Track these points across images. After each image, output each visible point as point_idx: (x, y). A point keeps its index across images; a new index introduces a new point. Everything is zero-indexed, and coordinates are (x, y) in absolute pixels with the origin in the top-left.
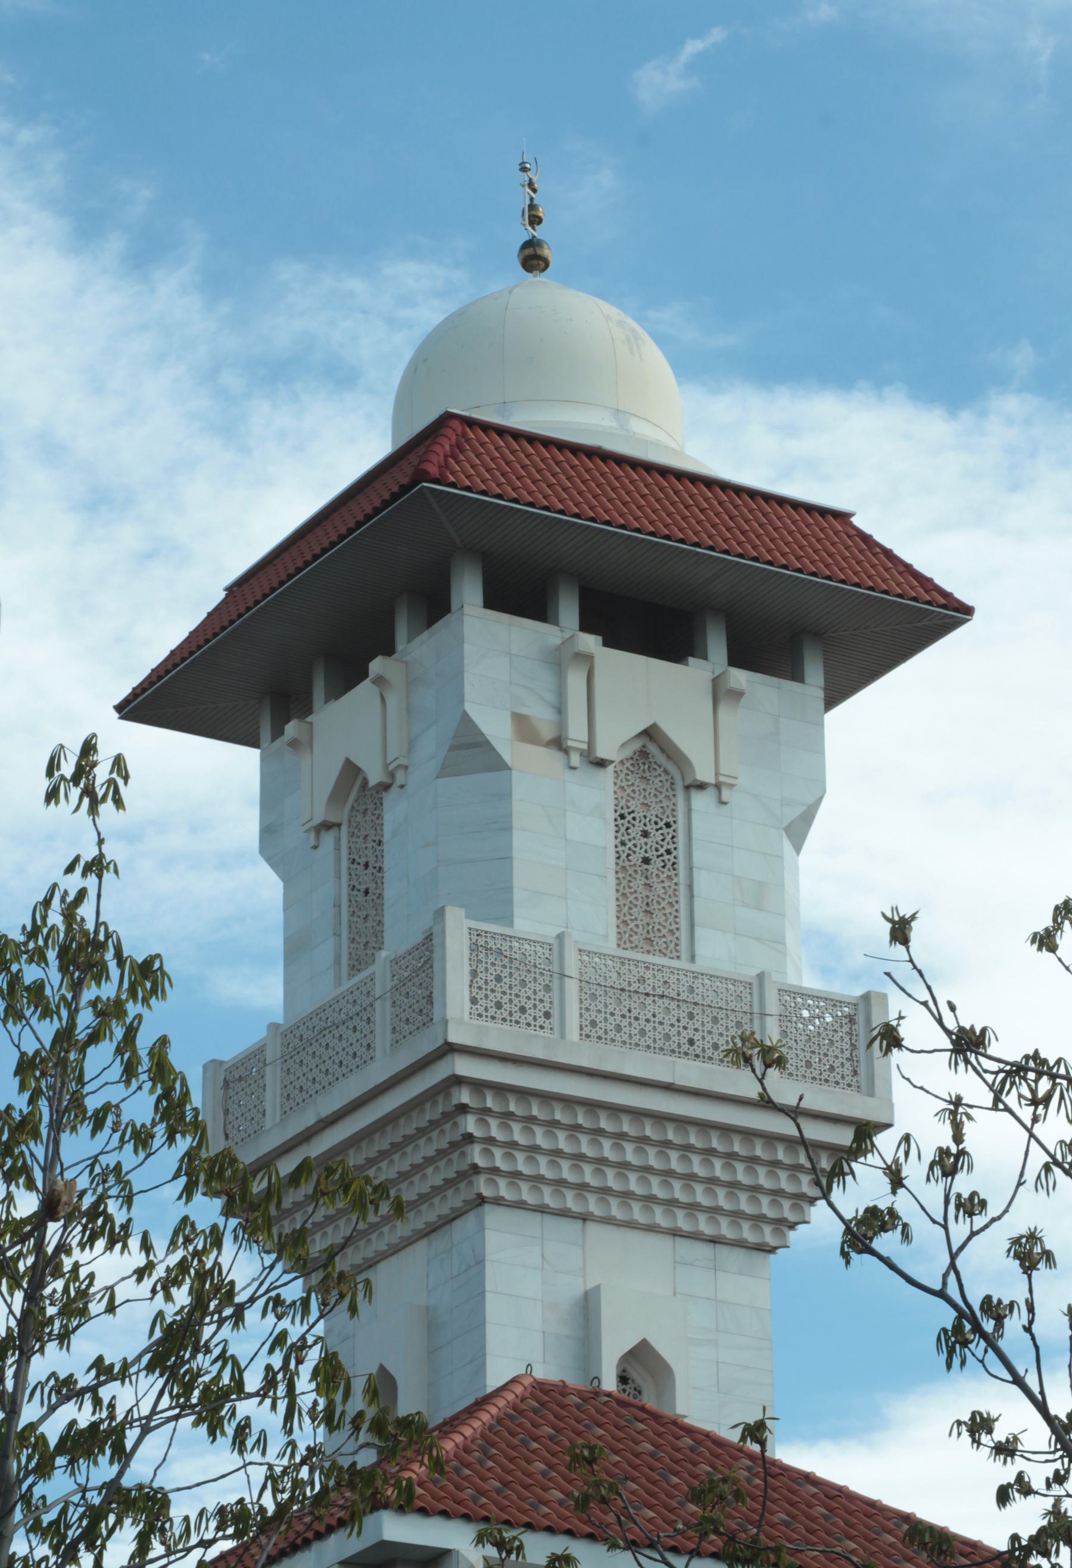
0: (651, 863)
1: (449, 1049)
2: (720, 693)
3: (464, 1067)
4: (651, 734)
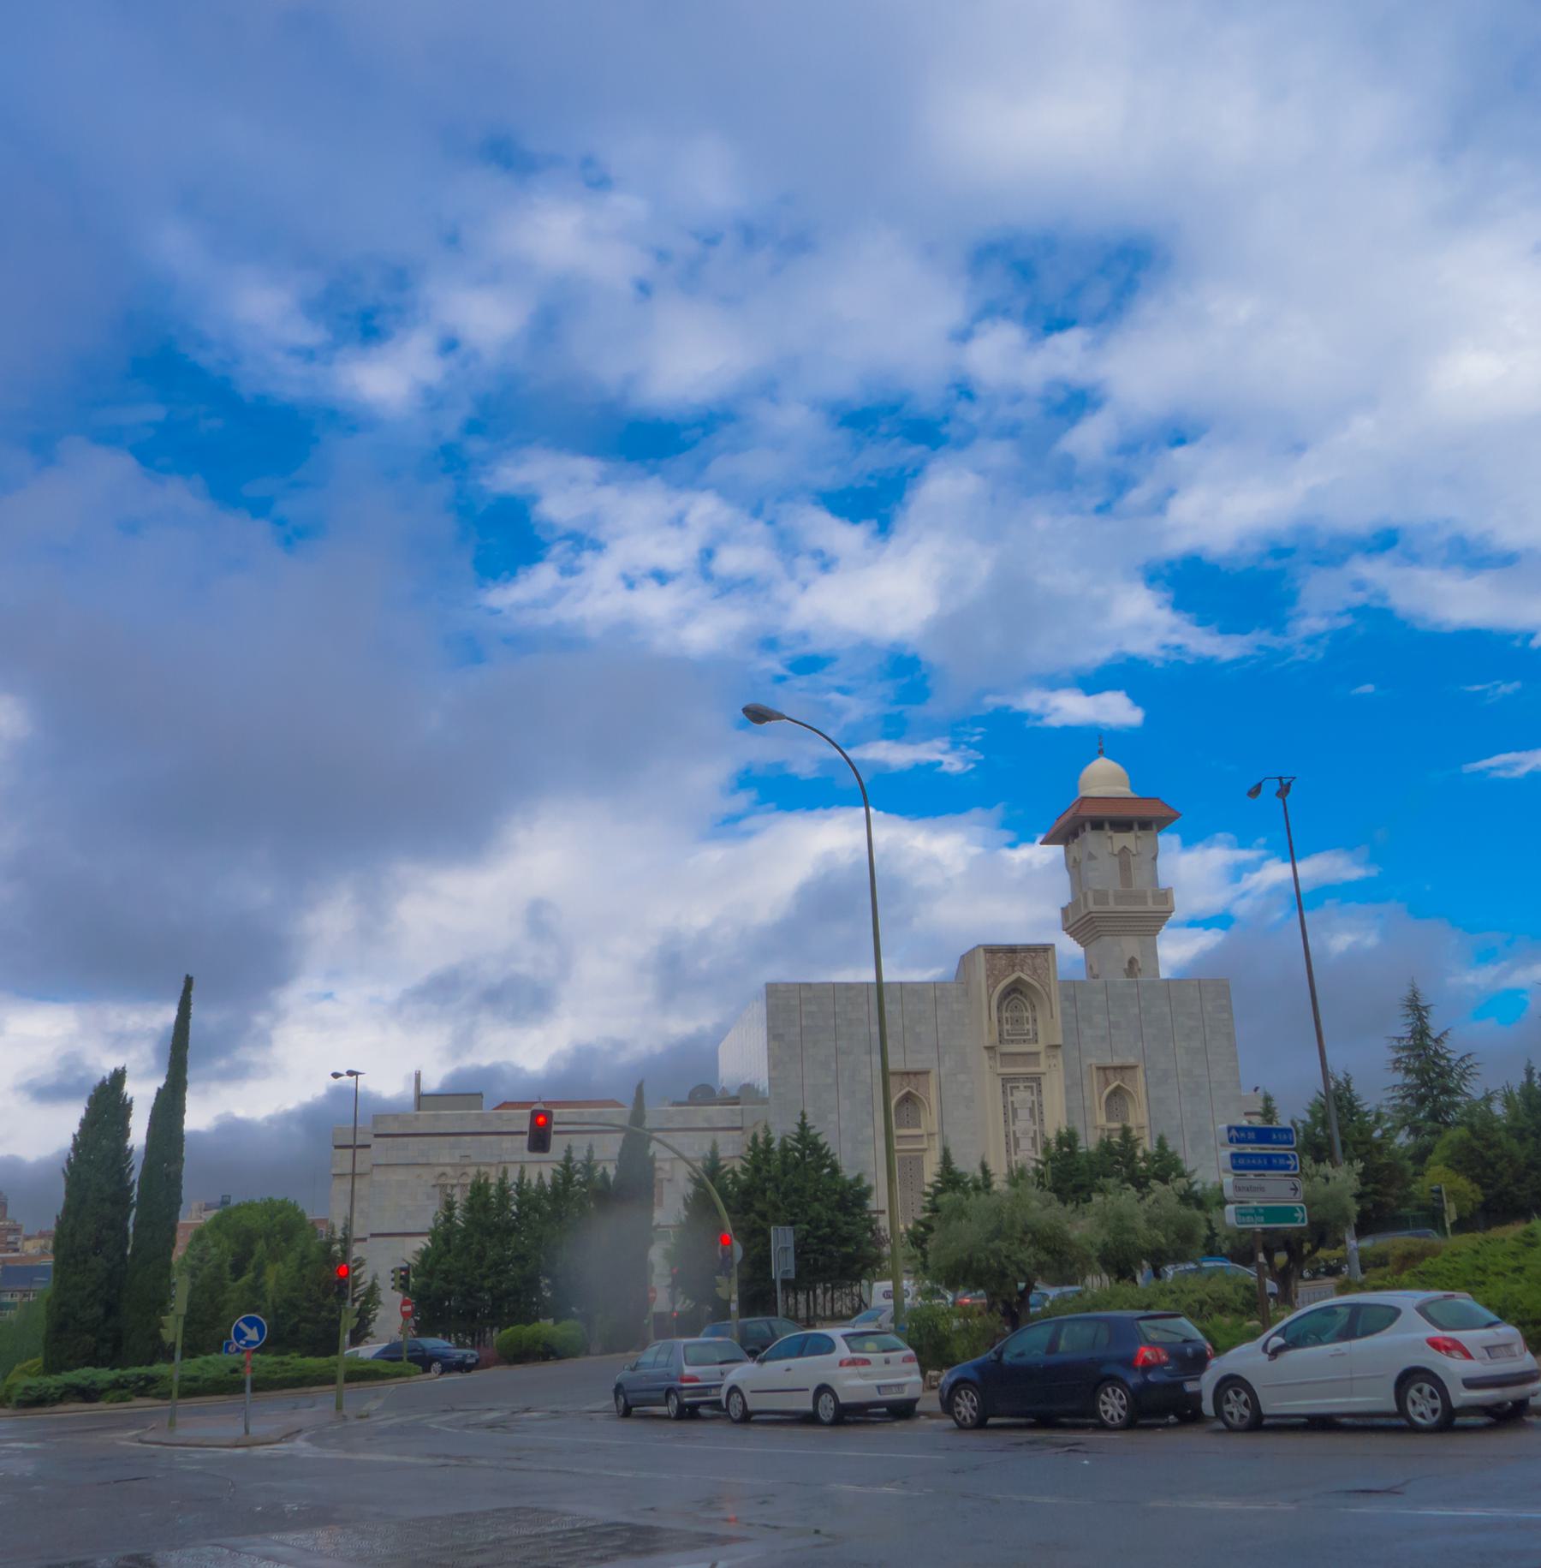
0: (1125, 868)
2: (1137, 837)
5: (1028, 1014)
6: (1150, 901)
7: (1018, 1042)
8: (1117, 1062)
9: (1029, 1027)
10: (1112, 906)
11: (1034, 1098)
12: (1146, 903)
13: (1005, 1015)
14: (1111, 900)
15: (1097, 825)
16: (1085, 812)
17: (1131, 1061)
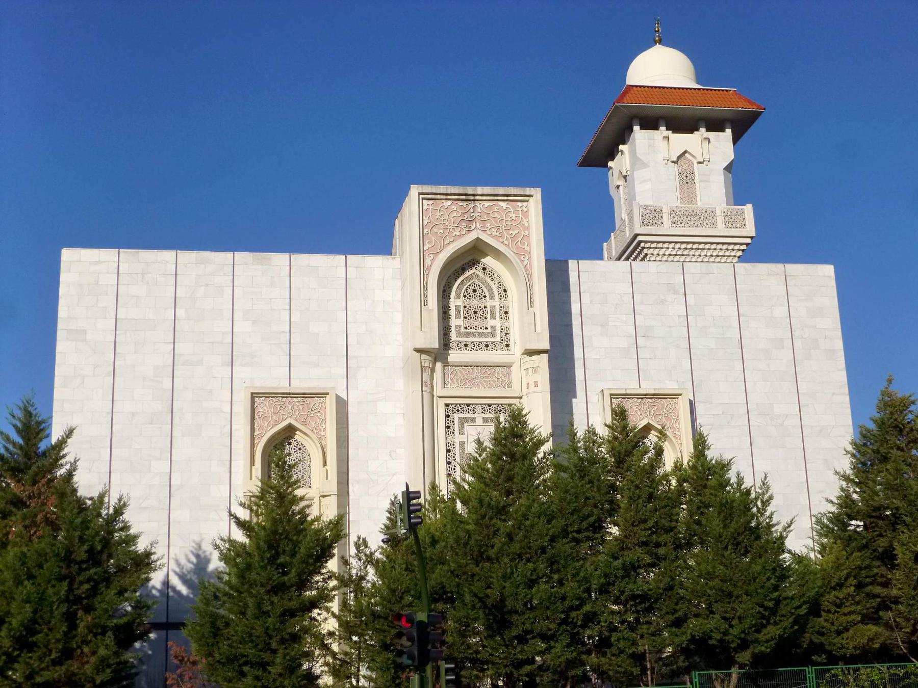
1: (636, 235)
3: (640, 238)
4: (685, 152)
5: (496, 303)
6: (720, 221)
7: (477, 346)
8: (647, 387)
9: (496, 322)
10: (667, 228)
12: (714, 225)
13: (454, 302)
14: (666, 218)
15: (650, 124)
16: (631, 102)
17: (669, 387)
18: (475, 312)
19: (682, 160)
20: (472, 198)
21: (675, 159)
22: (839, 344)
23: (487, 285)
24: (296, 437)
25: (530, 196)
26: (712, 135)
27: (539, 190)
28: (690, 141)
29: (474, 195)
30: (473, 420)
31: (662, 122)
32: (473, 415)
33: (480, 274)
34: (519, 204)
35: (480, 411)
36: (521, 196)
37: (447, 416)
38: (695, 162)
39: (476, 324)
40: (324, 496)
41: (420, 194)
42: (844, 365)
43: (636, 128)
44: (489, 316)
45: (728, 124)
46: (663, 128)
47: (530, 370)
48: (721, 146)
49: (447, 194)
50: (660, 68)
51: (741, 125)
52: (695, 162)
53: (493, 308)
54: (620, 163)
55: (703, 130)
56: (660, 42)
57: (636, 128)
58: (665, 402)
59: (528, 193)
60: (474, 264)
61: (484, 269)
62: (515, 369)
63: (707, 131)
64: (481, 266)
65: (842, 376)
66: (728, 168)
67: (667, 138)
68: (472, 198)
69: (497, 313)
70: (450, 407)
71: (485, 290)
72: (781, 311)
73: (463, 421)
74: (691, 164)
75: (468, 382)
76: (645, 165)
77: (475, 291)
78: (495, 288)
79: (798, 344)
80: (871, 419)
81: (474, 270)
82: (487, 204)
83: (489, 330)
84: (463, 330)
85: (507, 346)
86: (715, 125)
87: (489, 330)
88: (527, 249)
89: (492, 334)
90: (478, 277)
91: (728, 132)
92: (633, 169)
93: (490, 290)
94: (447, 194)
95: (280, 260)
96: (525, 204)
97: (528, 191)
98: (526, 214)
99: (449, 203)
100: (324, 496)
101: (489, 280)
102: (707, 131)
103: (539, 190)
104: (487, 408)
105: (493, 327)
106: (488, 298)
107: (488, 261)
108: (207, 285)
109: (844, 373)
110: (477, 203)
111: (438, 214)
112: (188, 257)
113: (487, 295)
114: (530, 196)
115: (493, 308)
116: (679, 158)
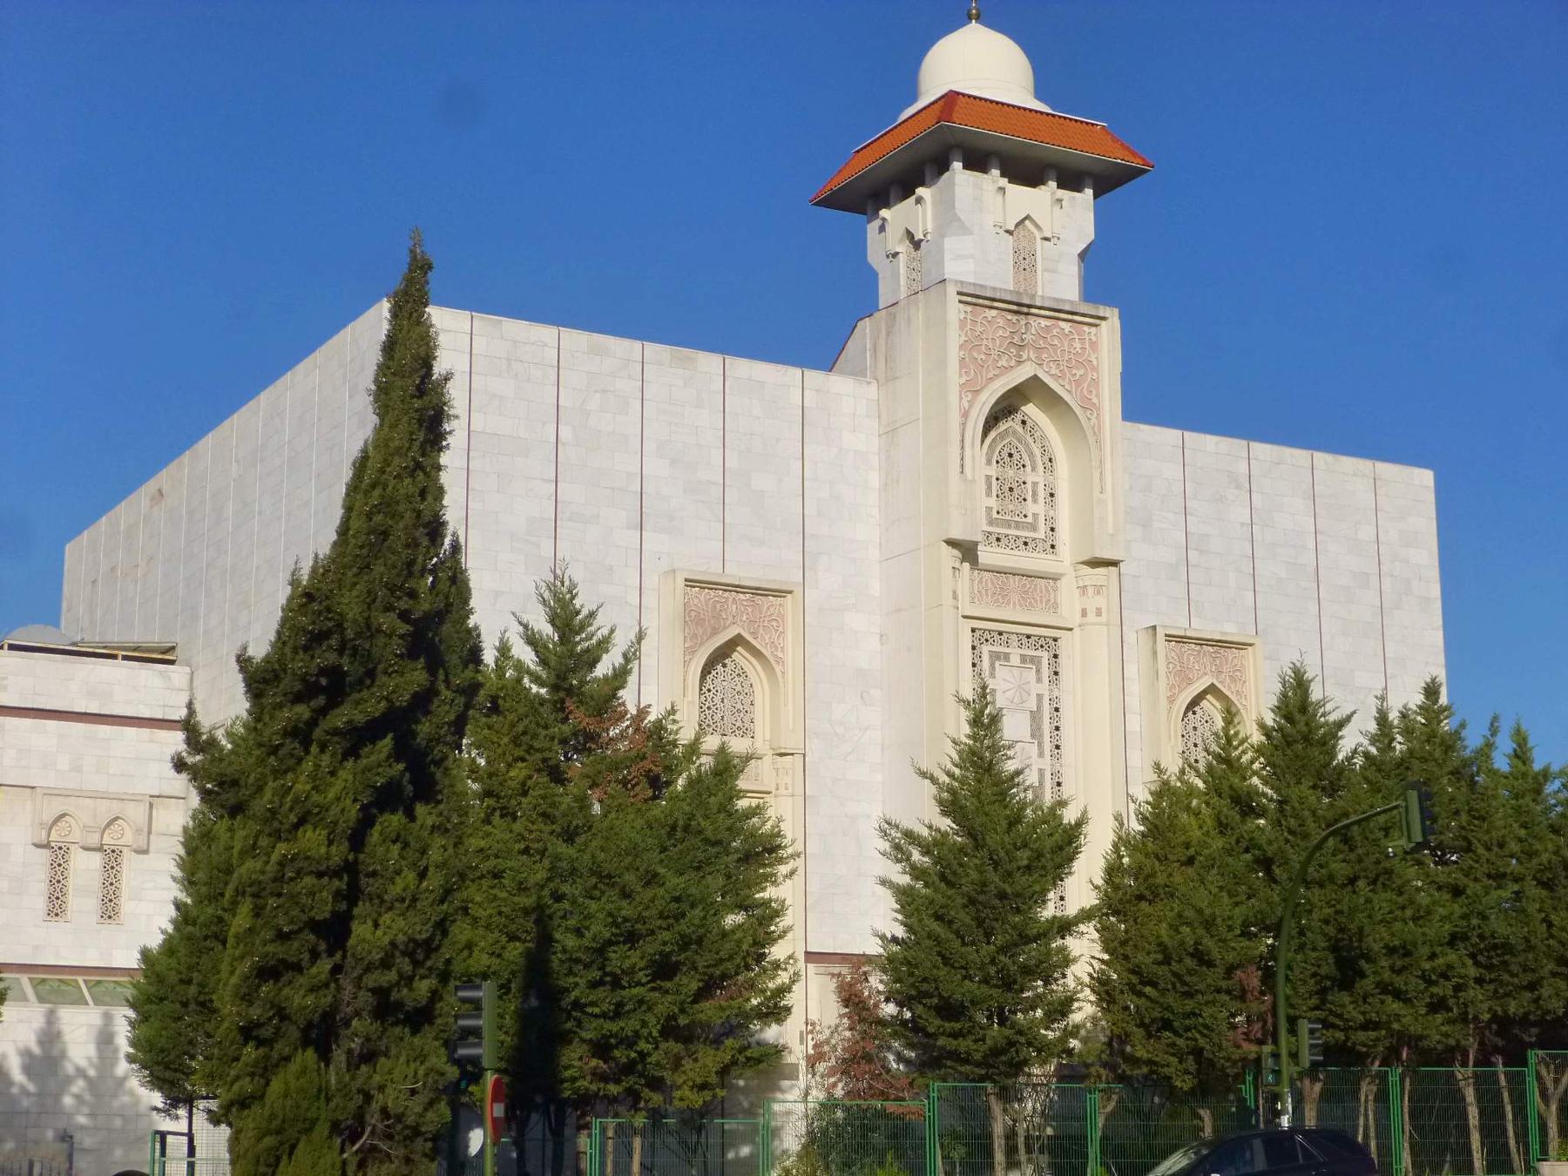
4: (1027, 217)
11: (1044, 688)
15: (977, 162)
16: (962, 122)
17: (1230, 631)
18: (1011, 489)
19: (1021, 231)
20: (1025, 310)
21: (1012, 228)
22: (1435, 591)
23: (1027, 445)
24: (735, 655)
25: (1104, 318)
26: (1065, 194)
27: (1116, 311)
28: (1041, 200)
29: (1029, 306)
30: (1007, 657)
31: (994, 161)
32: (1007, 650)
33: (1019, 428)
34: (1086, 328)
35: (1016, 644)
36: (1092, 316)
37: (974, 648)
38: (1038, 235)
39: (1011, 507)
40: (781, 755)
41: (959, 293)
42: (1440, 622)
43: (957, 165)
44: (1029, 498)
45: (1089, 181)
46: (996, 172)
47: (1090, 590)
48: (1069, 218)
49: (994, 300)
50: (979, 64)
51: (1105, 181)
52: (1038, 235)
53: (1035, 484)
54: (916, 213)
55: (1053, 184)
56: (978, 19)
57: (957, 165)
58: (1231, 654)
59: (1101, 314)
60: (1010, 413)
61: (1024, 422)
62: (1064, 584)
63: (1059, 187)
64: (1019, 417)
65: (1438, 638)
66: (1082, 256)
67: (1002, 189)
68: (1025, 310)
69: (1042, 494)
70: (977, 634)
71: (1025, 456)
72: (1367, 533)
73: (995, 656)
74: (1032, 240)
75: (1002, 597)
76: (965, 230)
77: (1011, 455)
78: (1037, 452)
79: (1387, 584)
80: (1299, 684)
81: (1010, 423)
82: (1044, 322)
83: (1030, 519)
84: (995, 515)
85: (1053, 547)
86: (1071, 180)
87: (1030, 519)
88: (1095, 400)
89: (1034, 528)
90: (1015, 432)
91: (1089, 192)
92: (941, 233)
93: (1031, 455)
94: (994, 300)
95: (709, 363)
96: (1093, 330)
97: (1103, 311)
98: (1094, 346)
99: (994, 313)
100: (781, 755)
101: (1031, 440)
102: (1059, 187)
103: (1116, 311)
104: (1025, 640)
105: (1035, 515)
106: (1028, 468)
107: (1030, 410)
108: (605, 391)
109: (1441, 634)
110: (1031, 319)
111: (979, 329)
112: (576, 339)
113: (1028, 463)
114: (1104, 318)
115: (1035, 484)
116: (1017, 225)
